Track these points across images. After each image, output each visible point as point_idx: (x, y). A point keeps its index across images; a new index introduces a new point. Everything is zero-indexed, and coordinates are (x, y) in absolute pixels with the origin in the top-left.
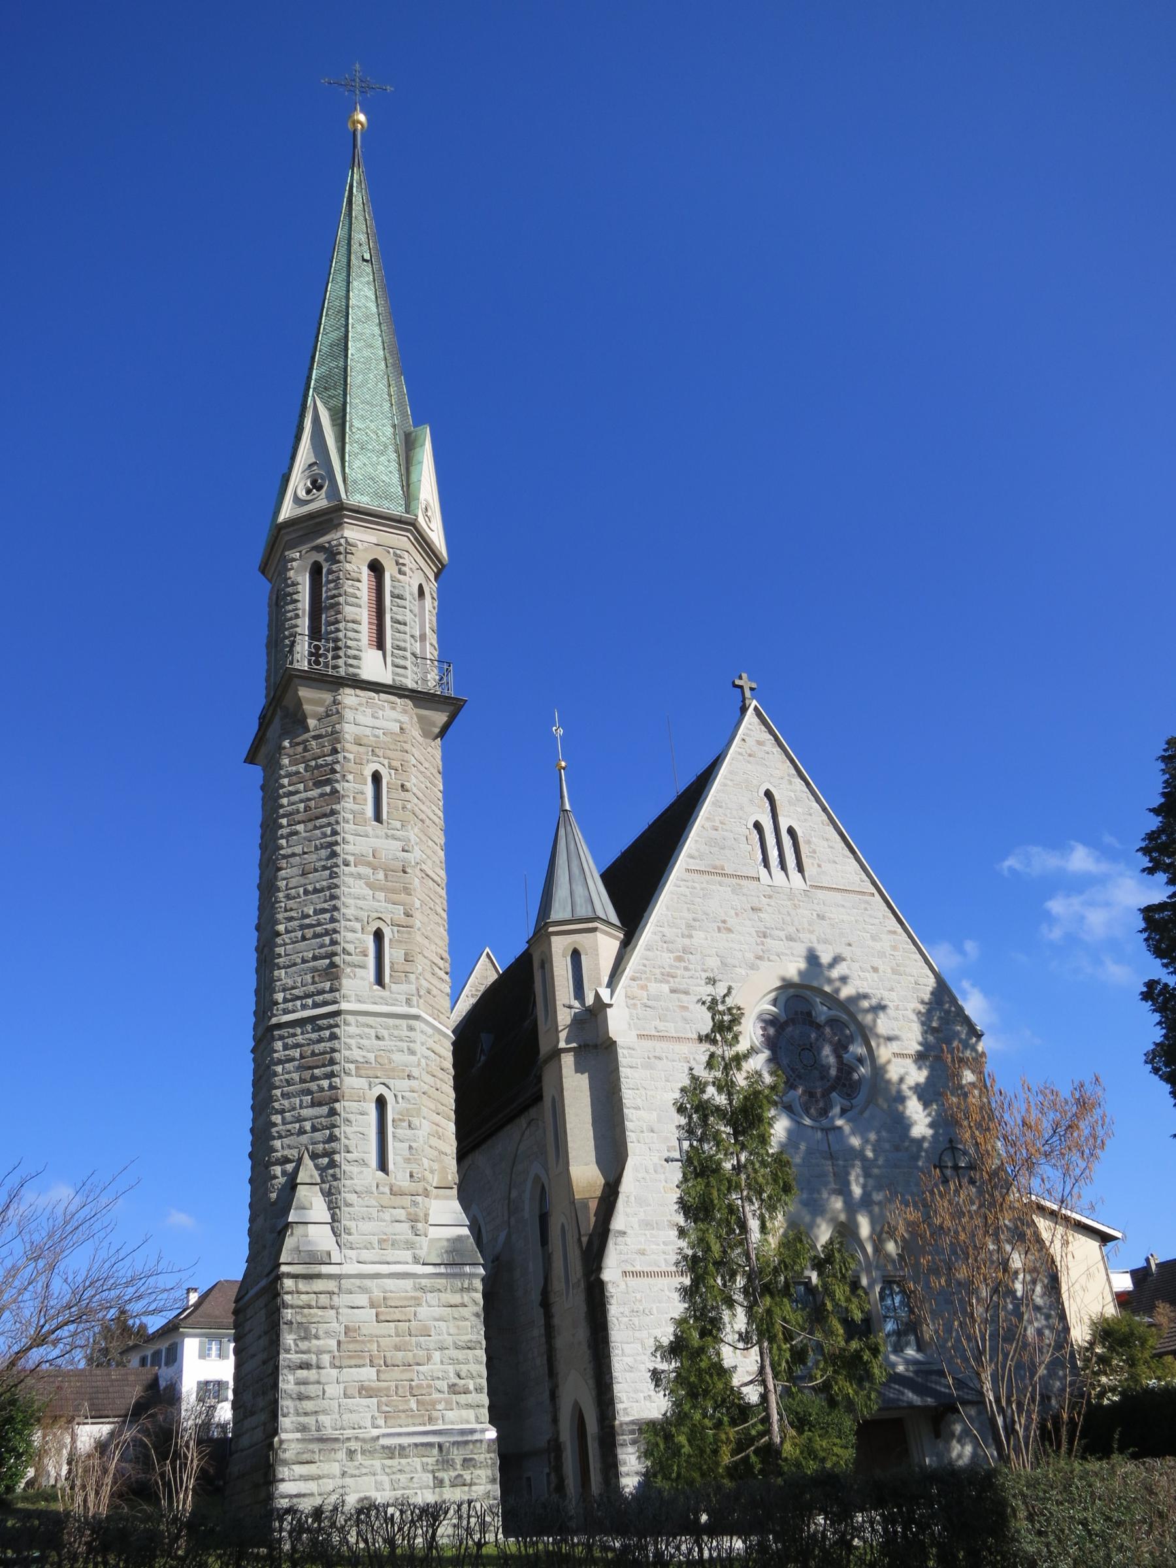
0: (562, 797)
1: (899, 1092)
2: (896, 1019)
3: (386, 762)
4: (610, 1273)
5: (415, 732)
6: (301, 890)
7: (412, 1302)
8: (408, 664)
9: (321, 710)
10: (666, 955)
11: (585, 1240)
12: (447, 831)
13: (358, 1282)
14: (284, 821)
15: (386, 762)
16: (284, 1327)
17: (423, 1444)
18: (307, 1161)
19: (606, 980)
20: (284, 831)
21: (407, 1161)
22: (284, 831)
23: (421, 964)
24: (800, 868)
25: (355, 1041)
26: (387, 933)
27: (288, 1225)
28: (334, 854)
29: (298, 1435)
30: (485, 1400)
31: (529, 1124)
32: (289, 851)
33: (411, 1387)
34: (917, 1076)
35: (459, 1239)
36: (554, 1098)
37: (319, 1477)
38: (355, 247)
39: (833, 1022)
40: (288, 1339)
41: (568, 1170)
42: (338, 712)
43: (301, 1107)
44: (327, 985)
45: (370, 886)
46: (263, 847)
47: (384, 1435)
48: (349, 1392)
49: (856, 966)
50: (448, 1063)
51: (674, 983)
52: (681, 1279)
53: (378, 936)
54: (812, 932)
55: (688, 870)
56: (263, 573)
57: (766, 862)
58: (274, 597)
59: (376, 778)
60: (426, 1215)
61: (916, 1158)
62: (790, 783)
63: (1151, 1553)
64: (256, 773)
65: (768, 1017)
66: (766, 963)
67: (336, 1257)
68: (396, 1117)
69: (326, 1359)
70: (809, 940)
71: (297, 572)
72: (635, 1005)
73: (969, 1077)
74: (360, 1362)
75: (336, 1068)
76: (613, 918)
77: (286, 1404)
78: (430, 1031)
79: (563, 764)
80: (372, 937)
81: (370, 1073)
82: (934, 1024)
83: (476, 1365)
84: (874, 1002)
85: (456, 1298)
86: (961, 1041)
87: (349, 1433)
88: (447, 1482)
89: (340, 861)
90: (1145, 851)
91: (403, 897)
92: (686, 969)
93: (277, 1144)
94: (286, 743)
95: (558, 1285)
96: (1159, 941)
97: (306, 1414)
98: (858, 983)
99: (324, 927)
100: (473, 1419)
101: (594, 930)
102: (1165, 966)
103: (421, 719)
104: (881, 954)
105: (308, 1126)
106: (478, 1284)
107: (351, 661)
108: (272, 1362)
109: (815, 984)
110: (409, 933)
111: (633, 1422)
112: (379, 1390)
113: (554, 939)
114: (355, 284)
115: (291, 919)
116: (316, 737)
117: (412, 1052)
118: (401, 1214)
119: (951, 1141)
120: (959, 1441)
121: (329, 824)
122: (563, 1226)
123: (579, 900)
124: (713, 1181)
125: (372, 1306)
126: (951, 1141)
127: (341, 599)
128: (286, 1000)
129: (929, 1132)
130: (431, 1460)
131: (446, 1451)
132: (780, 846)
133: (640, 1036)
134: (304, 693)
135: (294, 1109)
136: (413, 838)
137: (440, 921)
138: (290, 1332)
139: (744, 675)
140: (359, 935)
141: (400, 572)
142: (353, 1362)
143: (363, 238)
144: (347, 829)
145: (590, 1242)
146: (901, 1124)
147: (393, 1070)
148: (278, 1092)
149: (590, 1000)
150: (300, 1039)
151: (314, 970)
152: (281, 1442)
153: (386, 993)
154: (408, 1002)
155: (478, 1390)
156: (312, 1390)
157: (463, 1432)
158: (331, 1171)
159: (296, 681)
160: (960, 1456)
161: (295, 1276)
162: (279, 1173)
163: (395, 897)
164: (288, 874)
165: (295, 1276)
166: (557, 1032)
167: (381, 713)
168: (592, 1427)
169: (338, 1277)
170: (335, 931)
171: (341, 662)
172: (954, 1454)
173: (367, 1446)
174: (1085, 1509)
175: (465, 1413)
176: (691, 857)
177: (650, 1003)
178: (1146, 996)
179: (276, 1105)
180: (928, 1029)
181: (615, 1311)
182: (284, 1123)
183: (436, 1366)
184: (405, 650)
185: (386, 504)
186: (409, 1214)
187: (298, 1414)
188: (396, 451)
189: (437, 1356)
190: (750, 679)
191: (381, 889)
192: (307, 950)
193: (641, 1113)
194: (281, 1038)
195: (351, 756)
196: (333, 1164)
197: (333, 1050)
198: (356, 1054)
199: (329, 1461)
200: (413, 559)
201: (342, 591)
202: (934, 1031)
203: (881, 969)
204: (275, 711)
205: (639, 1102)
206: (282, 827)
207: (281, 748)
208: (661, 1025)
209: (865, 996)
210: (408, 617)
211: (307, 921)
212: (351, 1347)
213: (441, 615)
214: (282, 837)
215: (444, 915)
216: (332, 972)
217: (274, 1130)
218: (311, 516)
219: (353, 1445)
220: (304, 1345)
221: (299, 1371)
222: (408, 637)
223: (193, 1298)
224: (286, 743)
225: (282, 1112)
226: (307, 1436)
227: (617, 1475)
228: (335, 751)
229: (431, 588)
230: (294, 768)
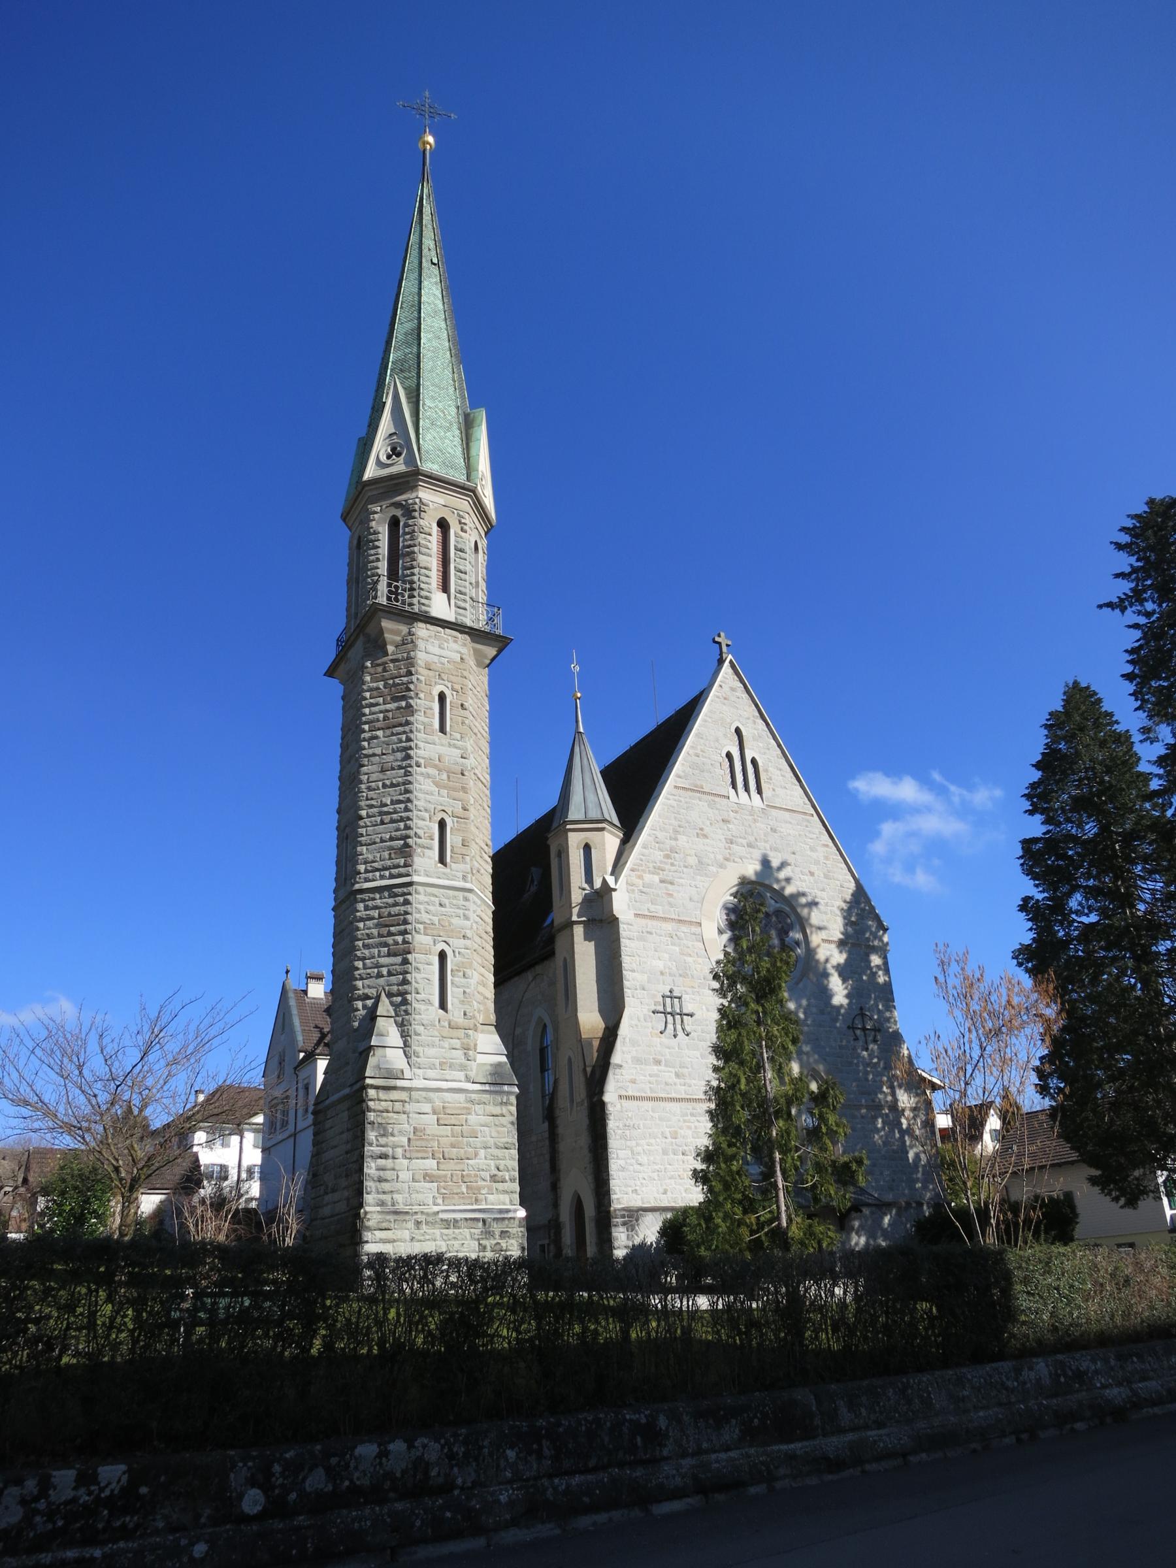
0: (577, 722)
1: (825, 969)
2: (826, 913)
3: (449, 685)
4: (610, 1096)
5: (472, 662)
6: (380, 784)
7: (464, 1112)
8: (467, 606)
9: (399, 639)
10: (658, 853)
11: (589, 1070)
12: (492, 744)
13: (424, 1094)
14: (366, 727)
15: (449, 685)
16: (368, 1126)
17: (471, 1219)
18: (384, 999)
19: (610, 869)
20: (366, 735)
21: (462, 1002)
22: (366, 735)
23: (474, 849)
24: (760, 792)
25: (424, 907)
26: (449, 821)
27: (370, 1048)
28: (408, 757)
29: (378, 1209)
30: (516, 1187)
31: (534, 978)
32: (370, 752)
33: (463, 1176)
34: (839, 958)
35: (499, 1064)
36: (565, 959)
37: (394, 1241)
38: (425, 251)
39: (778, 912)
40: (371, 1135)
41: (576, 1015)
42: (412, 642)
43: (379, 956)
44: (402, 861)
45: (437, 784)
46: (344, 747)
48: (416, 1177)
49: (797, 870)
50: (490, 929)
51: (662, 875)
53: (442, 824)
54: (766, 842)
55: (676, 787)
56: (344, 520)
57: (734, 785)
58: (355, 542)
59: (442, 697)
60: (476, 1045)
61: (836, 1020)
62: (754, 722)
63: (1095, 1312)
64: (335, 688)
65: (731, 906)
66: (732, 864)
67: (407, 1074)
69: (399, 1151)
70: (764, 847)
71: (378, 523)
73: (876, 960)
75: (408, 927)
76: (616, 821)
77: (369, 1184)
78: (479, 902)
79: (579, 695)
80: (437, 826)
81: (435, 932)
82: (853, 919)
83: (510, 1161)
84: (810, 899)
85: (497, 1110)
86: (871, 933)
87: (416, 1208)
88: (489, 1248)
89: (413, 763)
92: (672, 864)
93: (359, 984)
94: (368, 664)
95: (563, 1101)
96: (1031, 867)
97: (384, 1193)
98: (798, 883)
99: (400, 815)
100: (508, 1201)
101: (603, 829)
102: (1037, 886)
103: (475, 650)
104: (817, 862)
105: (385, 971)
106: (513, 1100)
107: (423, 601)
108: (357, 1153)
109: (767, 882)
111: (623, 1209)
112: (439, 1177)
113: (570, 834)
114: (425, 283)
115: (371, 806)
116: (393, 661)
117: (466, 918)
118: (456, 1043)
119: (861, 1009)
120: (857, 1233)
121: (405, 732)
122: (570, 1059)
123: (590, 805)
124: (744, 1033)
125: (434, 1113)
126: (861, 1009)
127: (416, 549)
128: (367, 871)
129: (845, 1001)
130: (477, 1231)
131: (486, 1224)
132: (744, 773)
133: (637, 915)
134: (386, 624)
135: (373, 957)
136: (469, 748)
138: (373, 1130)
139: (722, 634)
140: (427, 823)
141: (462, 530)
142: (420, 1155)
143: (432, 246)
144: (419, 737)
145: (593, 1072)
146: (826, 994)
147: (452, 931)
148: (360, 943)
149: (598, 884)
150: (378, 902)
151: (391, 848)
152: (366, 1213)
153: (447, 870)
154: (464, 878)
155: (512, 1180)
156: (388, 1175)
157: (501, 1211)
158: (403, 1008)
159: (380, 613)
160: (857, 1244)
161: (377, 1088)
162: (360, 1007)
163: (455, 794)
164: (369, 770)
165: (377, 1088)
166: (571, 908)
168: (590, 1211)
169: (409, 1089)
170: (409, 819)
171: (415, 601)
172: (853, 1243)
173: (430, 1219)
174: (1058, 1279)
175: (501, 1197)
176: (679, 776)
177: (645, 890)
179: (358, 953)
180: (848, 923)
181: (612, 1125)
182: (365, 968)
183: (481, 1161)
184: (465, 594)
185: (452, 472)
186: (462, 1043)
187: (378, 1193)
188: (460, 429)
189: (482, 1152)
190: (727, 637)
191: (445, 788)
192: (386, 831)
193: (635, 974)
194: (363, 901)
195: (422, 678)
196: (405, 1002)
197: (406, 913)
198: (425, 917)
199: (401, 1229)
200: (471, 520)
201: (416, 542)
202: (852, 924)
203: (816, 873)
204: (358, 636)
205: (634, 966)
206: (364, 731)
207: (364, 667)
208: (652, 908)
209: (804, 894)
210: (468, 568)
211: (385, 809)
212: (419, 1143)
213: (490, 567)
214: (364, 740)
215: (489, 810)
216: (406, 851)
217: (357, 973)
218: (391, 477)
219: (420, 1217)
220: (383, 1141)
221: (379, 1160)
222: (467, 584)
223: (201, 1098)
224: (368, 664)
225: (363, 959)
226: (386, 1209)
227: (611, 1248)
228: (410, 673)
229: (483, 544)
230: (375, 685)
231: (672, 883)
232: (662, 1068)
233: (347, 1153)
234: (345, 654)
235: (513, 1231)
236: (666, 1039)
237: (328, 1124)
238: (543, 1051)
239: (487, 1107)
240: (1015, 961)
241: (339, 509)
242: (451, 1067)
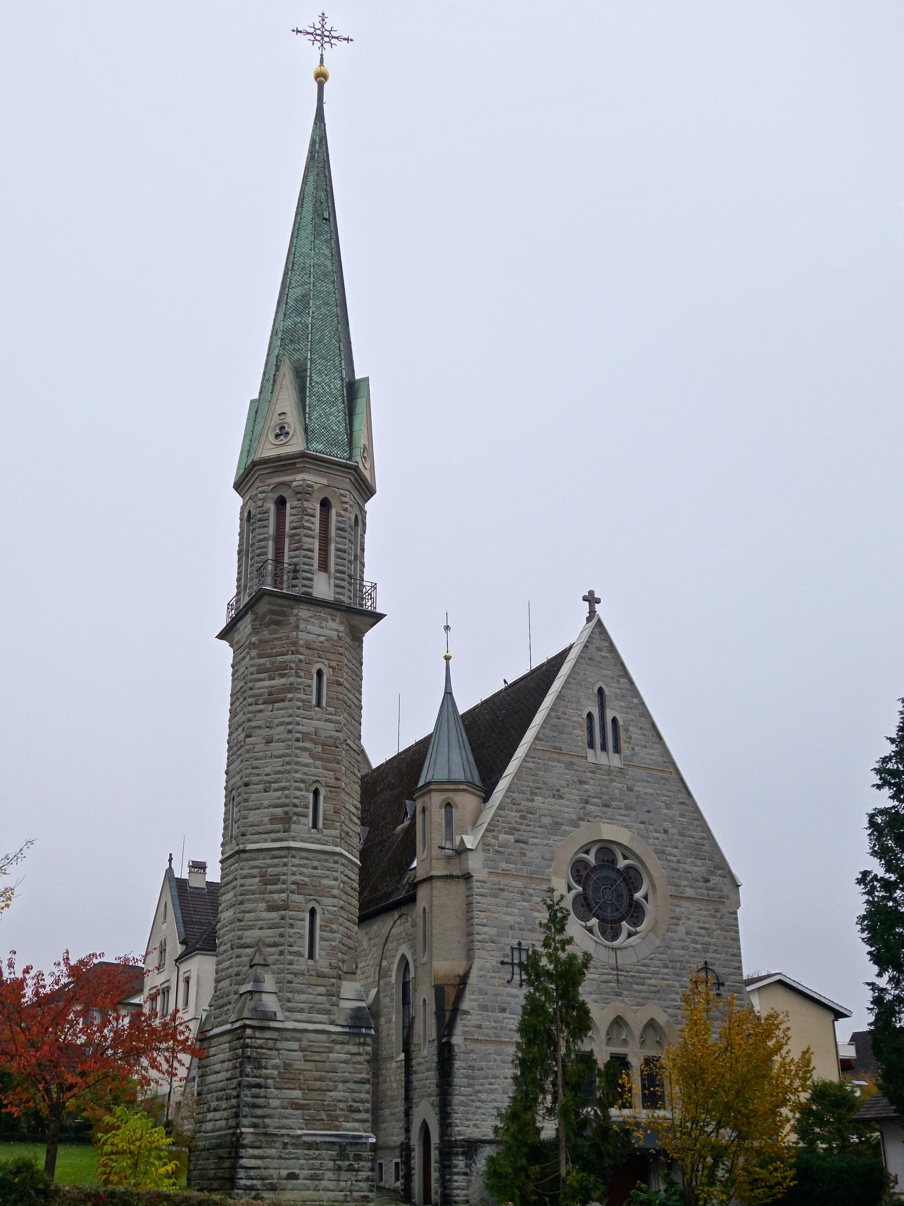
3: (326, 662)
17: (329, 1142)
24: (617, 749)
29: (252, 1130)
31: (400, 917)
45: (312, 756)
52: (515, 1071)
54: (621, 801)
56: (236, 490)
59: (320, 673)
67: (280, 1016)
68: (323, 923)
72: (489, 850)
74: (292, 1086)
78: (347, 863)
80: (312, 794)
81: (307, 892)
85: (354, 1049)
87: (283, 1131)
90: (878, 771)
91: (334, 765)
110: (336, 792)
111: (463, 1140)
122: (424, 1000)
137: (355, 779)
157: (354, 1137)
167: (324, 623)
178: (860, 882)
186: (327, 990)
187: (252, 1117)
193: (487, 929)
203: (671, 831)
204: (246, 613)
212: (287, 1076)
231: (526, 843)
232: (506, 1015)
233: (227, 1080)
234: (236, 624)
235: (364, 1154)
237: (213, 1051)
238: (405, 985)
239: (346, 1047)
240: (859, 927)
241: (232, 478)
242: (319, 1012)
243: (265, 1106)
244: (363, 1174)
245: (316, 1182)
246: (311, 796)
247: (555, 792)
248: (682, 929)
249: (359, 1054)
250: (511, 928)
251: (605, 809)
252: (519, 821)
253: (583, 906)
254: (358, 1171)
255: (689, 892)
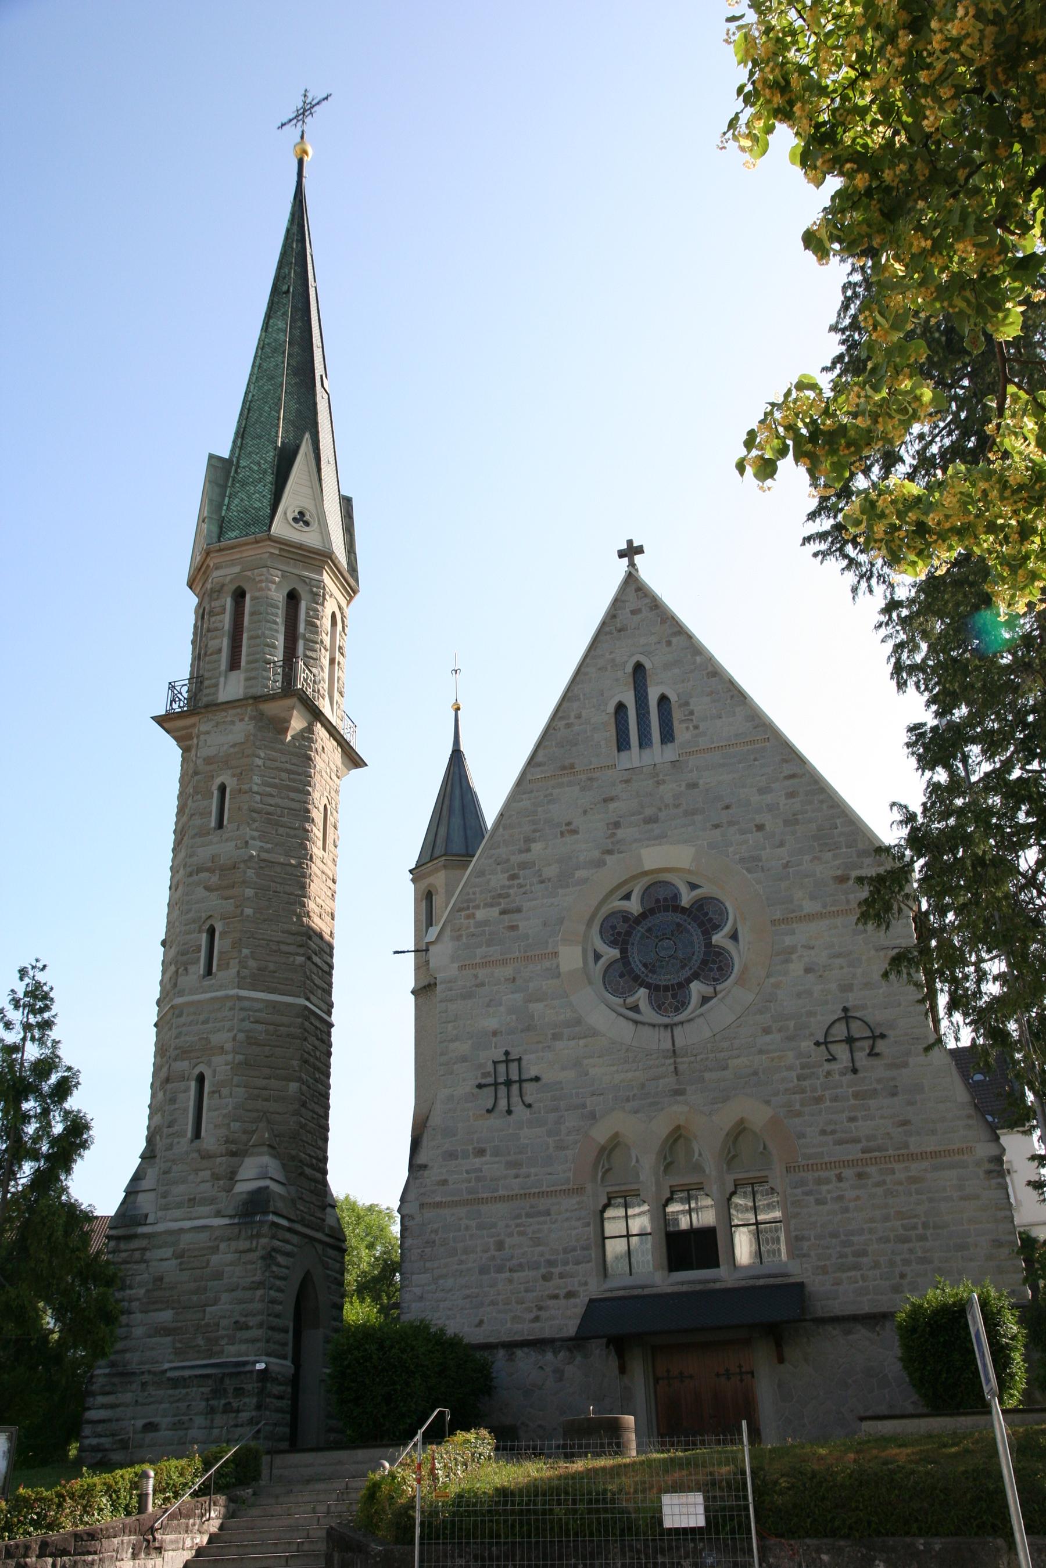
26: (219, 928)
47: (171, 1369)
51: (504, 904)
56: (191, 588)
59: (222, 789)
69: (135, 1304)
87: (147, 1367)
178: (911, 730)
219: (146, 1378)
232: (487, 1158)
235: (249, 1387)
236: (495, 1121)
243: (126, 1338)
244: (245, 1416)
245: (181, 1433)
246: (204, 936)
247: (564, 828)
248: (796, 968)
249: (250, 1250)
250: (495, 1034)
251: (650, 826)
252: (507, 883)
253: (622, 976)
254: (238, 1411)
255: (809, 907)
